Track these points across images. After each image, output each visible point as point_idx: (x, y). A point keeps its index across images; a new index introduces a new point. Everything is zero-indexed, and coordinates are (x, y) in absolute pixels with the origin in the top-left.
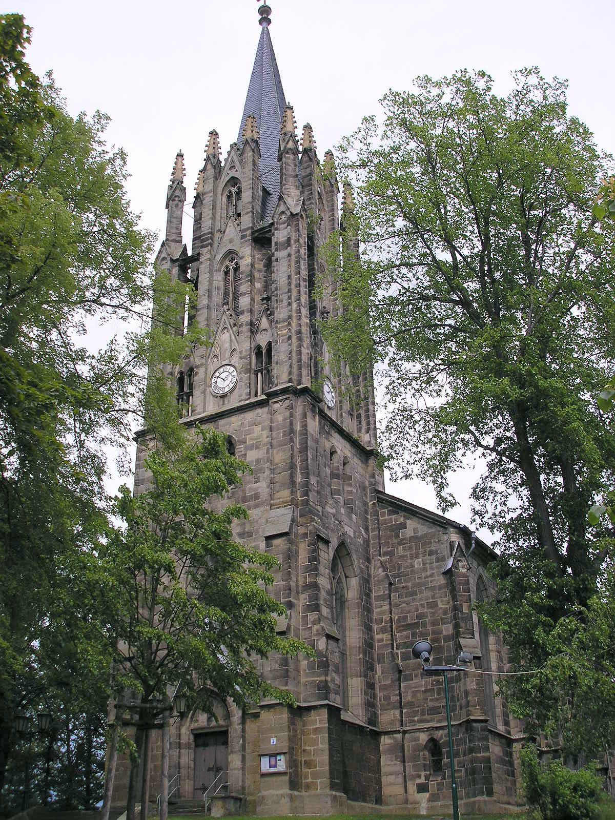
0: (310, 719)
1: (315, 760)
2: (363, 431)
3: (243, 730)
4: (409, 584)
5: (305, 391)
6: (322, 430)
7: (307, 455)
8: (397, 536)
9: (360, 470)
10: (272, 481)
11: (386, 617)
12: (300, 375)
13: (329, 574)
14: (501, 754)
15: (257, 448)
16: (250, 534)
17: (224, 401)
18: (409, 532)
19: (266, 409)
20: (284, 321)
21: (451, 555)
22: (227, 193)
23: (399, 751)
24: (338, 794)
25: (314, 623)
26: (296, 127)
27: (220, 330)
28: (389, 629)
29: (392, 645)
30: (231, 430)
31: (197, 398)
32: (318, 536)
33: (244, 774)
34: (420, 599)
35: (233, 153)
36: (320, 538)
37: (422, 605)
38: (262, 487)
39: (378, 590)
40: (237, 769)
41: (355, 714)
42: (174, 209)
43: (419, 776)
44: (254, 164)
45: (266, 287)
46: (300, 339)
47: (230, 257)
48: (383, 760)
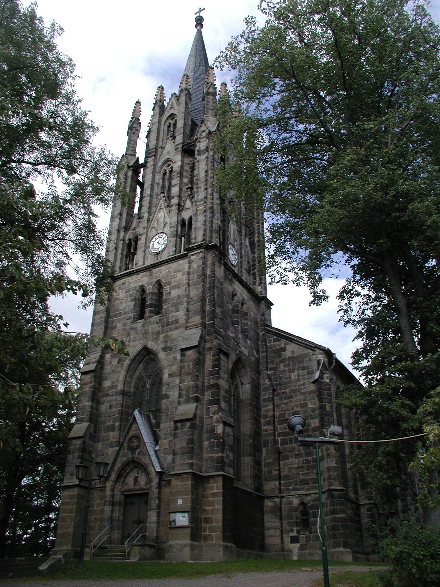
0: (209, 485)
1: (212, 518)
2: (257, 284)
3: (159, 493)
4: (287, 391)
5: (214, 247)
6: (226, 278)
7: (214, 292)
8: (279, 356)
9: (254, 310)
10: (188, 310)
11: (270, 414)
12: (211, 237)
13: (227, 378)
14: (352, 515)
15: (178, 287)
16: (171, 349)
17: (157, 257)
18: (288, 354)
19: (186, 261)
20: (201, 201)
21: (318, 369)
22: (167, 124)
23: (278, 511)
24: (229, 545)
25: (214, 413)
26: (215, 80)
27: (158, 210)
28: (272, 422)
29: (275, 434)
30: (161, 276)
31: (139, 257)
32: (220, 349)
33: (158, 527)
34: (296, 401)
35: (173, 99)
36: (221, 351)
37: (297, 406)
38: (181, 315)
39: (265, 395)
40: (153, 522)
41: (247, 484)
42: (132, 135)
43: (292, 531)
44: (186, 104)
45: (191, 181)
46: (212, 213)
47: (167, 164)
48: (266, 517)
